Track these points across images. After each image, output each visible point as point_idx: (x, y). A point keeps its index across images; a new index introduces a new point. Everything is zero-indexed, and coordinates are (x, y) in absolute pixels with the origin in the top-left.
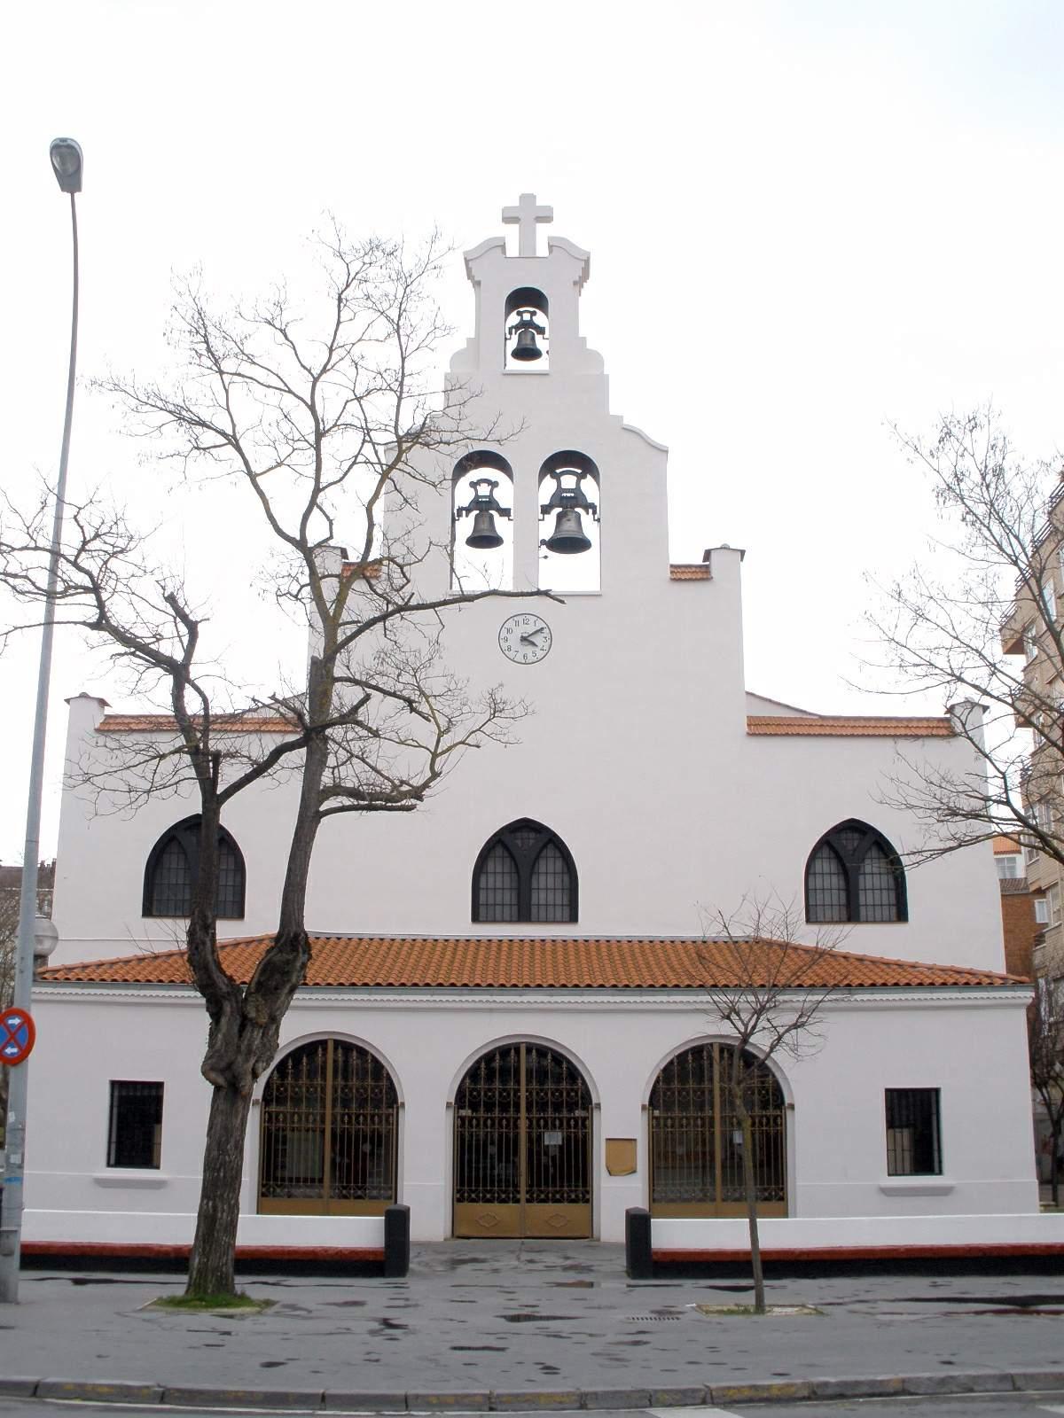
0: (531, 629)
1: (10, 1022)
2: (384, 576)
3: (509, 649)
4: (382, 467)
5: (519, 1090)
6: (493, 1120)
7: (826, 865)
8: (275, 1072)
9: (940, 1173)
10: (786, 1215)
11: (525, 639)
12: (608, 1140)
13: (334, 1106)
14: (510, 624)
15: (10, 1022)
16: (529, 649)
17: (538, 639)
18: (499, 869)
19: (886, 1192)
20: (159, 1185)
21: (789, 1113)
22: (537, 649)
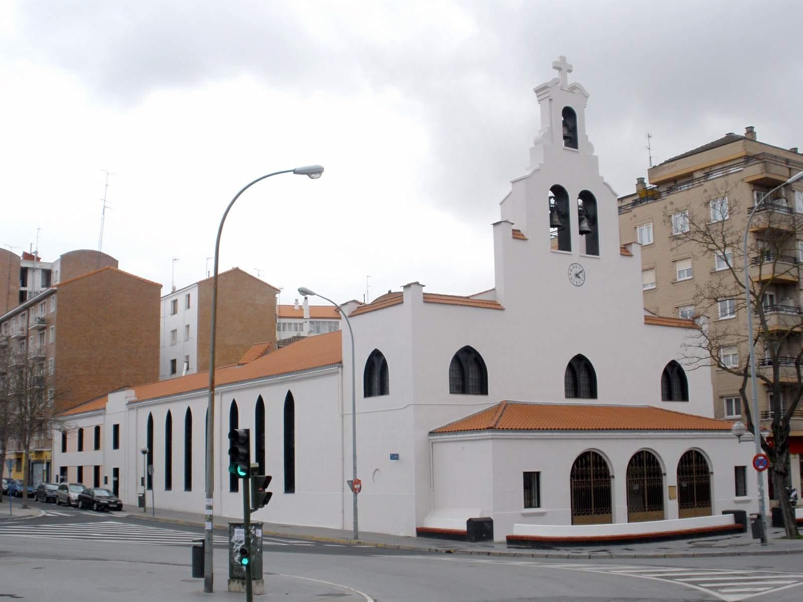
0: (578, 271)
1: (760, 458)
2: (700, 310)
3: (572, 279)
4: (754, 304)
5: (644, 469)
6: (602, 481)
7: (356, 306)
8: (575, 465)
9: (539, 506)
10: (611, 522)
11: (577, 275)
12: (669, 487)
13: (594, 478)
14: (571, 268)
15: (760, 458)
16: (578, 280)
17: (580, 275)
18: (584, 376)
19: (524, 515)
20: (543, 514)
21: (711, 475)
22: (580, 280)
